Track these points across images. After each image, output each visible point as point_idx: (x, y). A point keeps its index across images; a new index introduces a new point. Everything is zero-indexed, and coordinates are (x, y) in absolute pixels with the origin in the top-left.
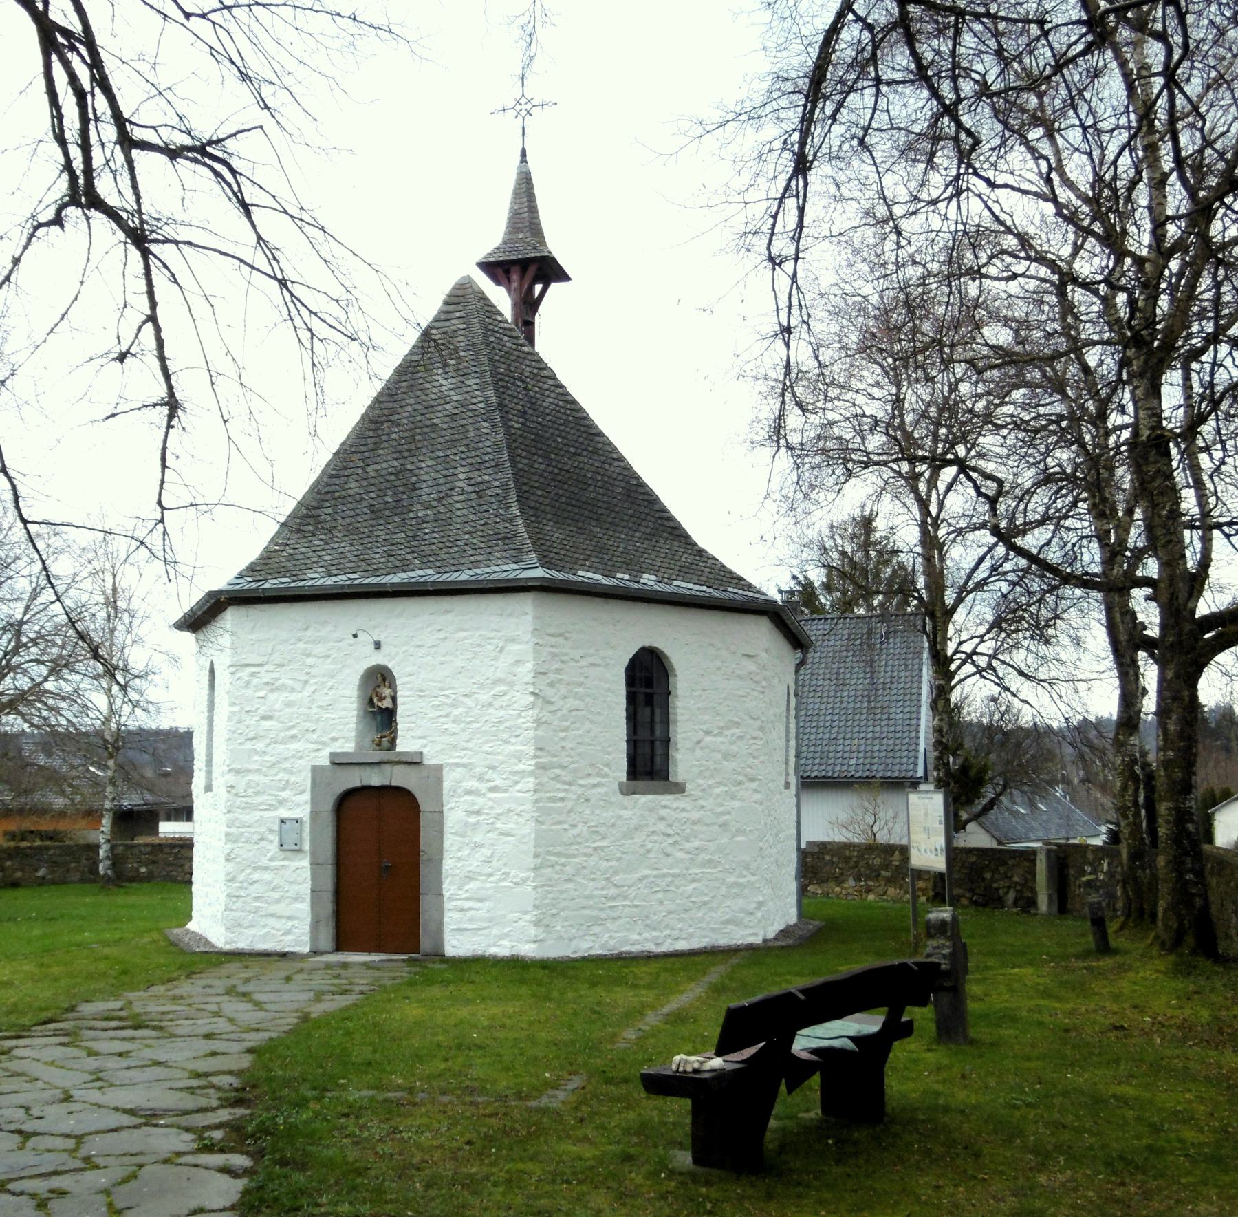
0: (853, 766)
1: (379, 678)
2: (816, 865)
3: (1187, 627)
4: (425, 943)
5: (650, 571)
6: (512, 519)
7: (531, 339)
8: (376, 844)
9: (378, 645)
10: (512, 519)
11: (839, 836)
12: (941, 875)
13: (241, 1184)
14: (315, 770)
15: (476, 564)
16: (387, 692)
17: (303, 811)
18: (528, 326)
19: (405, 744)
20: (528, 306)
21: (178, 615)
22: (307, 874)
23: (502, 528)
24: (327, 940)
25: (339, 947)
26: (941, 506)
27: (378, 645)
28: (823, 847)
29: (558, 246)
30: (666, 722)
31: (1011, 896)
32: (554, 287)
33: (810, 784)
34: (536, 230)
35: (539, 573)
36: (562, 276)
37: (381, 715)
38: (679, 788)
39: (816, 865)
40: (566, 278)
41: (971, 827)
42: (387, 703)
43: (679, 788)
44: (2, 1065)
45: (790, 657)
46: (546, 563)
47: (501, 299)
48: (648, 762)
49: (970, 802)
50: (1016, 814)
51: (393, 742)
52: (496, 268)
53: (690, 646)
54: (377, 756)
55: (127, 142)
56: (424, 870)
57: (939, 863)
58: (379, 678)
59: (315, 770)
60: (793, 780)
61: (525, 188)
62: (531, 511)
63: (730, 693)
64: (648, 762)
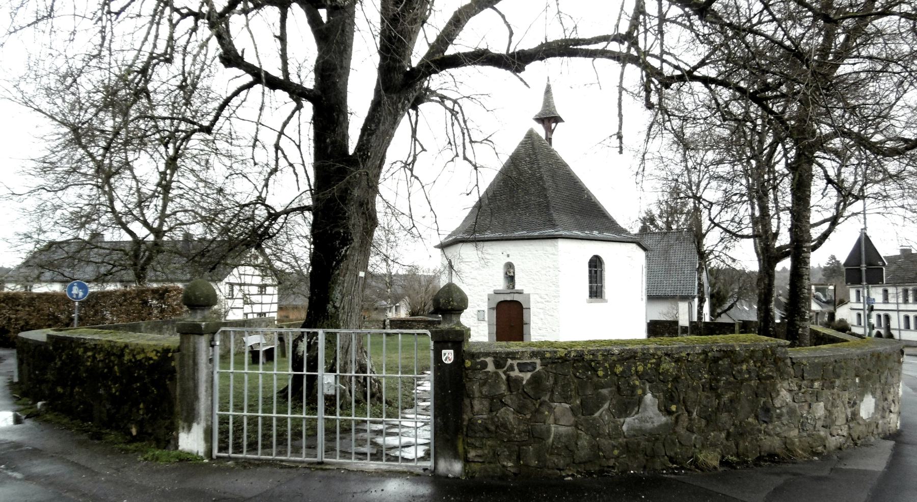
0: (669, 292)
1: (509, 266)
7: (550, 143)
8: (510, 315)
9: (508, 256)
12: (686, 327)
15: (540, 230)
17: (486, 308)
18: (549, 140)
19: (518, 287)
20: (550, 131)
21: (438, 243)
22: (487, 328)
27: (508, 256)
29: (560, 112)
32: (559, 124)
36: (561, 120)
37: (510, 279)
38: (606, 301)
39: (655, 328)
41: (723, 315)
43: (606, 301)
44: (915, 214)
47: (540, 130)
48: (596, 292)
49: (720, 305)
51: (514, 287)
52: (540, 120)
53: (607, 251)
54: (509, 291)
55: (471, 142)
57: (687, 324)
58: (509, 266)
59: (489, 295)
61: (548, 91)
64: (596, 292)
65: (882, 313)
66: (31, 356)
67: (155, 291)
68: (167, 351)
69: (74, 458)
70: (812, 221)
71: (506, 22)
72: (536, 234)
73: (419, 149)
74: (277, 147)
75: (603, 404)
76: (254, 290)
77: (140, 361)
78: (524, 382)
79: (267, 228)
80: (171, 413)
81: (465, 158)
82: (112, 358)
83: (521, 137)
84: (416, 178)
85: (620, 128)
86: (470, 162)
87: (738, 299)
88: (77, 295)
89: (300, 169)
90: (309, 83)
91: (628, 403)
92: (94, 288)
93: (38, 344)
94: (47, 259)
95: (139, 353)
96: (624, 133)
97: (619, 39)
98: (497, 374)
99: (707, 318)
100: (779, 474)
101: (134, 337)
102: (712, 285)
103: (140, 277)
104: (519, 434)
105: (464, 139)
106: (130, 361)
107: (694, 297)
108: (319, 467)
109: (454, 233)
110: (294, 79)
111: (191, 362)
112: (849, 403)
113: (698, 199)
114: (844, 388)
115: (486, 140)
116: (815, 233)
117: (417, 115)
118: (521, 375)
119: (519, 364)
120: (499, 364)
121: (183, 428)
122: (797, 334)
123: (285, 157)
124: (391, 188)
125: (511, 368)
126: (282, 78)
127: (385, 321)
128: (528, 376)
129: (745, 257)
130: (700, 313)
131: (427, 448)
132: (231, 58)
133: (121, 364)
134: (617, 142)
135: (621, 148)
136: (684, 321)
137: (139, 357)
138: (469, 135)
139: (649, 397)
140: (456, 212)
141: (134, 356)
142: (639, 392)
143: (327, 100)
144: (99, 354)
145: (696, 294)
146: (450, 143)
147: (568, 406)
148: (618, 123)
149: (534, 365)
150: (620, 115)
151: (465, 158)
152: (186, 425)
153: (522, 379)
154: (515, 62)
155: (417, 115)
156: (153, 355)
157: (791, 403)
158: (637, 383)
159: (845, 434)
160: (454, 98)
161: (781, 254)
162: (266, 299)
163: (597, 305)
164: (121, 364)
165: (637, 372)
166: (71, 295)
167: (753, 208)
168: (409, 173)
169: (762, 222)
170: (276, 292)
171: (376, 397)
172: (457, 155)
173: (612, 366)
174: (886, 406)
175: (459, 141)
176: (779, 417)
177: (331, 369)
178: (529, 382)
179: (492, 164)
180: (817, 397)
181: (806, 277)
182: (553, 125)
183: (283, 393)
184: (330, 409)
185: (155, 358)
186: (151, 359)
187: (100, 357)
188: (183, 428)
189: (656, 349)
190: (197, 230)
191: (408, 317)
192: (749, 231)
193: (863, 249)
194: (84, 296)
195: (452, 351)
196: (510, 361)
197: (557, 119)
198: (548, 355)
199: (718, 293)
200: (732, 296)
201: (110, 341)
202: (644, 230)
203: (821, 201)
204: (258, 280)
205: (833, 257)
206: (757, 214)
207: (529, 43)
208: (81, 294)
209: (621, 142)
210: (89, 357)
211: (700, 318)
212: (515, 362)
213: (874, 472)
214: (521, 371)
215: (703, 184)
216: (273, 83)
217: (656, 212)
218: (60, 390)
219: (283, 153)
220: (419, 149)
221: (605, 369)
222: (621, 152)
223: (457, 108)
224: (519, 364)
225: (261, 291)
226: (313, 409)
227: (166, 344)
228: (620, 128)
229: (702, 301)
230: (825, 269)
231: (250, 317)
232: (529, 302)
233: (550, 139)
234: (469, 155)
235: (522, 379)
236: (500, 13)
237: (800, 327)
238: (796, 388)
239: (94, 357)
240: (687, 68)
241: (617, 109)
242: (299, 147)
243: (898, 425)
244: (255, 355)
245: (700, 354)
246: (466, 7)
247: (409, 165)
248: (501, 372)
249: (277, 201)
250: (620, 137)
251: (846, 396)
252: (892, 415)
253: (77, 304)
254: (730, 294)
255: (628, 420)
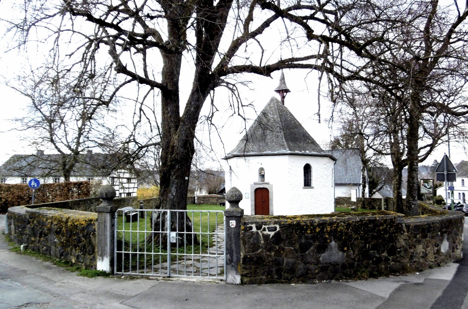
0: (347, 181)
1: (262, 169)
2: (338, 201)
3: (400, 161)
4: (270, 213)
5: (308, 150)
6: (284, 142)
7: (283, 104)
8: (262, 197)
10: (284, 142)
11: (343, 196)
13: (419, 147)
14: (251, 185)
15: (278, 150)
16: (263, 172)
18: (283, 101)
19: (266, 180)
20: (283, 97)
23: (282, 143)
24: (253, 213)
25: (255, 214)
26: (364, 131)
28: (340, 198)
29: (289, 87)
30: (311, 177)
31: (377, 207)
32: (288, 93)
33: (337, 185)
34: (284, 83)
35: (289, 152)
36: (290, 92)
38: (313, 188)
39: (338, 201)
40: (290, 92)
41: (376, 193)
42: (263, 174)
43: (313, 188)
45: (332, 162)
46: (290, 150)
48: (307, 183)
50: (387, 190)
53: (312, 162)
55: (242, 106)
56: (270, 202)
57: (355, 200)
58: (262, 169)
59: (251, 185)
60: (333, 185)
62: (287, 140)
63: (322, 170)
64: (307, 183)
65: (461, 192)
66: (17, 220)
67: (75, 184)
68: (91, 220)
69: (45, 275)
70: (419, 147)
71: (261, 46)
72: (276, 152)
73: (215, 110)
74: (141, 110)
75: (310, 247)
76: (125, 181)
77: (77, 225)
78: (271, 237)
79: (137, 154)
80: (93, 251)
81: (239, 115)
82: (62, 224)
83: (267, 101)
84: (213, 125)
85: (319, 110)
86: (242, 116)
87: (384, 184)
88: (34, 186)
89: (154, 124)
90: (159, 79)
91: (323, 247)
92: (42, 181)
93: (20, 216)
94: (16, 164)
95: (76, 221)
96: (321, 113)
97: (318, 57)
98: (257, 233)
99: (367, 196)
100: (398, 282)
101: (72, 213)
102: (370, 177)
103: (67, 177)
104: (269, 263)
105: (238, 105)
106: (72, 225)
107: (360, 185)
108: (168, 279)
109: (232, 151)
110: (151, 78)
111: (103, 226)
112: (435, 245)
113: (361, 134)
114: (432, 238)
115: (250, 104)
116: (422, 153)
117: (214, 93)
118: (269, 233)
119: (268, 228)
120: (259, 228)
121: (99, 260)
122: (411, 208)
123: (145, 114)
124: (201, 131)
125: (264, 230)
126: (145, 77)
127: (195, 197)
128: (272, 234)
129: (387, 162)
130: (363, 193)
131: (222, 269)
132: (122, 69)
133: (67, 227)
134: (317, 117)
135: (320, 120)
136: (354, 199)
137: (76, 224)
138: (241, 103)
139: (333, 243)
140: (234, 140)
141: (73, 223)
142: (329, 241)
143: (170, 93)
144: (55, 221)
145: (361, 182)
146: (231, 105)
147: (292, 248)
148: (318, 108)
149: (276, 228)
150: (319, 104)
151: (239, 115)
152: (101, 258)
153: (270, 235)
154: (266, 71)
155: (214, 93)
156: (83, 223)
157: (405, 245)
158: (327, 236)
159: (433, 260)
160: (233, 83)
161: (404, 163)
162: (132, 185)
163: (308, 190)
164: (67, 227)
165: (327, 230)
166: (31, 186)
167: (391, 138)
168: (209, 122)
169: (395, 145)
170: (136, 182)
171: (197, 243)
172: (235, 113)
173: (315, 228)
174: (455, 246)
175: (236, 105)
176: (399, 252)
177: (173, 230)
178: (273, 237)
179: (252, 116)
180: (419, 242)
181: (416, 178)
182: (285, 94)
183: (149, 241)
184: (172, 250)
185: (85, 224)
186: (82, 224)
187: (55, 223)
188: (99, 260)
189: (336, 219)
190: (97, 150)
191: (207, 194)
192: (389, 151)
193: (445, 163)
194: (37, 186)
195: (235, 221)
196: (264, 226)
197: (287, 91)
198: (282, 223)
199: (373, 180)
200: (381, 183)
201: (60, 215)
202: (334, 148)
203: (424, 141)
204: (127, 175)
205: (436, 161)
206: (393, 141)
207: (273, 61)
208: (36, 185)
209: (320, 117)
210: (49, 223)
211: (363, 196)
212: (266, 227)
213: (446, 281)
214: (269, 231)
215: (364, 125)
216: (142, 81)
217: (340, 138)
218: (33, 239)
219: (144, 112)
220: (215, 110)
221: (311, 230)
222: (320, 122)
223: (234, 88)
224: (268, 228)
225: (129, 181)
226: (165, 248)
227: (91, 217)
228: (319, 110)
229: (364, 187)
230: (432, 167)
231: (123, 196)
232: (272, 189)
233: (283, 101)
234: (241, 113)
235: (270, 235)
236: (257, 41)
237: (413, 204)
238: (408, 238)
239: (52, 223)
240: (355, 69)
241: (318, 101)
242: (154, 112)
243: (462, 255)
244: (128, 217)
245: (359, 221)
246: (248, 71)
247: (209, 118)
248: (259, 231)
249: (142, 141)
250: (319, 115)
251: (433, 241)
252: (458, 251)
253: (34, 191)
254: (380, 182)
255: (322, 255)
